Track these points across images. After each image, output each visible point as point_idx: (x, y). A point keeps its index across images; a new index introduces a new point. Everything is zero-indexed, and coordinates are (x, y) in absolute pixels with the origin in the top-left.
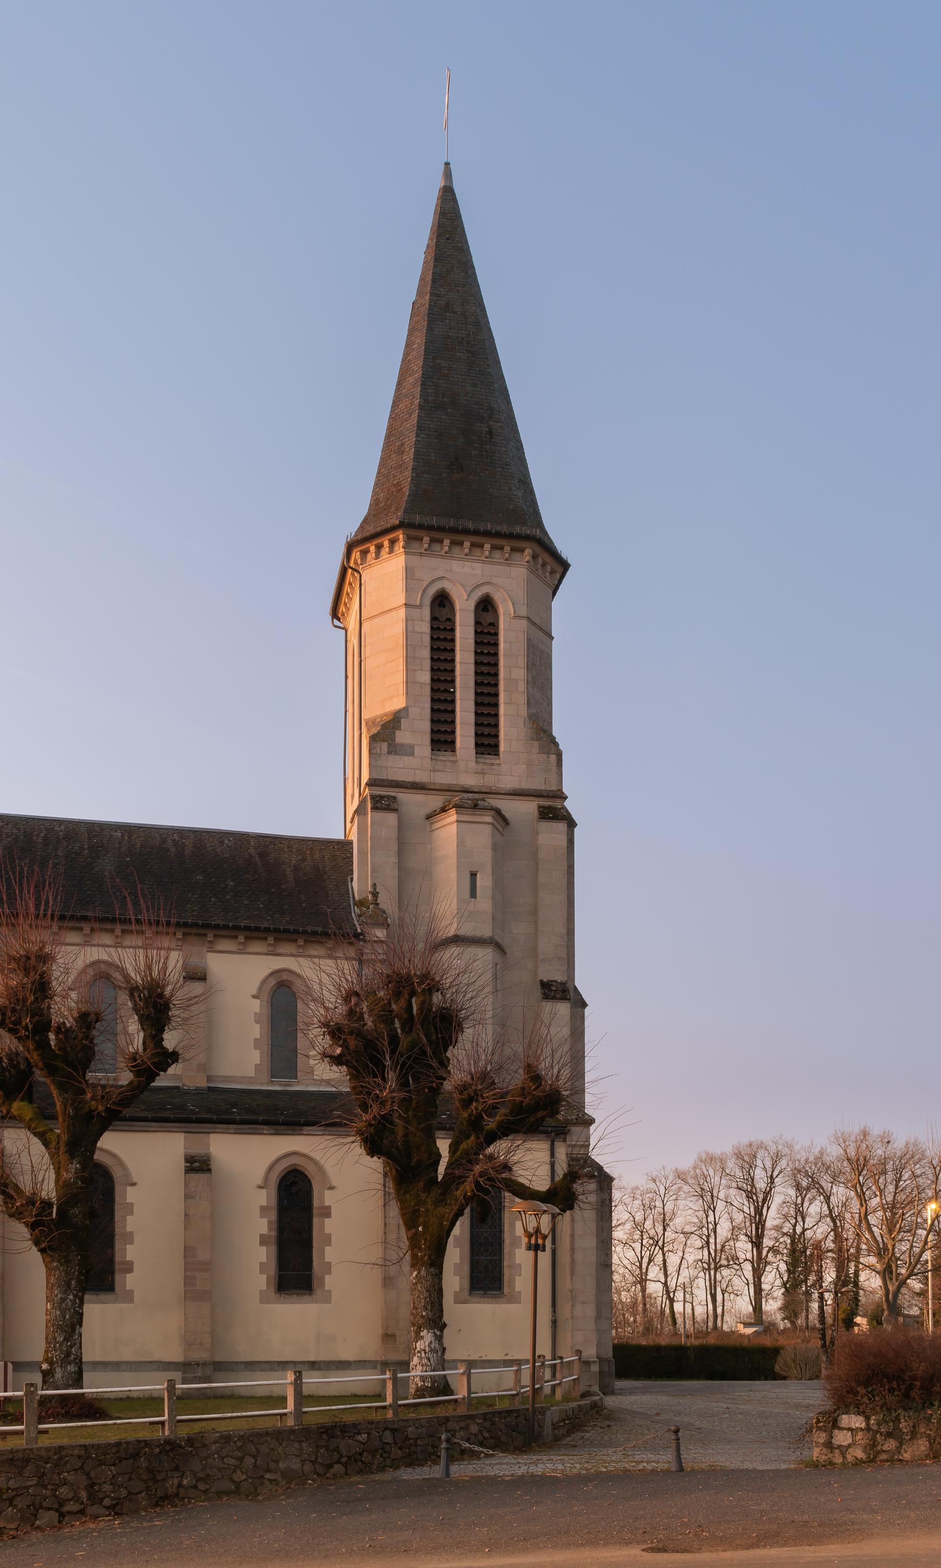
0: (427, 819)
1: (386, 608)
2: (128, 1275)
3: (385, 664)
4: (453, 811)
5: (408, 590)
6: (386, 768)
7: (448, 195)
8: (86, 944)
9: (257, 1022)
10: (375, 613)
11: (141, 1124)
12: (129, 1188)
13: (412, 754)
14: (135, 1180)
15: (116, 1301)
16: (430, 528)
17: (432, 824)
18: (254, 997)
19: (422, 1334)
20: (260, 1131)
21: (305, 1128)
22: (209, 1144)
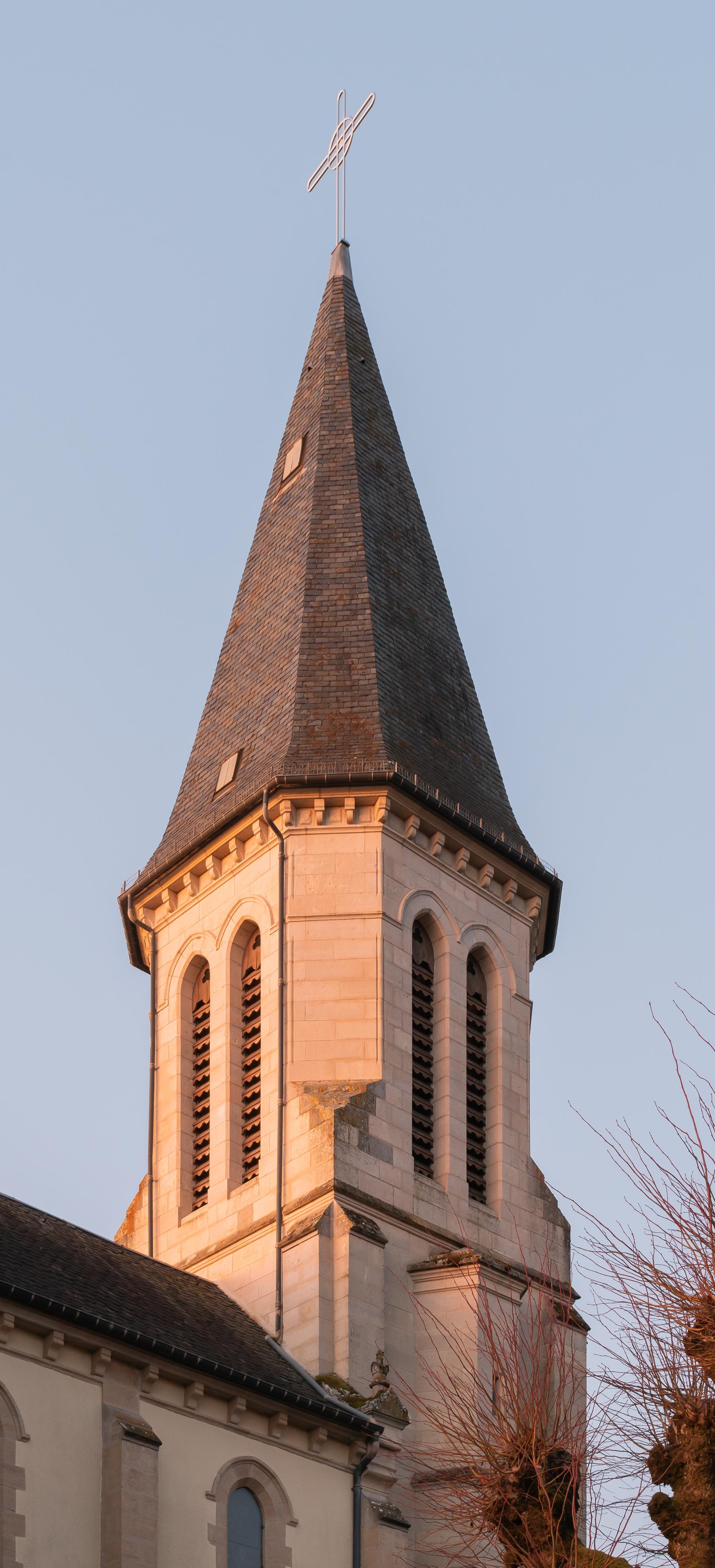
0: (410, 1272)
1: (340, 910)
3: (336, 1001)
4: (473, 1269)
5: (386, 893)
6: (357, 1170)
7: (343, 297)
9: (213, 1542)
10: (315, 911)
13: (390, 1161)
16: (430, 805)
17: (416, 1282)
18: (209, 1496)
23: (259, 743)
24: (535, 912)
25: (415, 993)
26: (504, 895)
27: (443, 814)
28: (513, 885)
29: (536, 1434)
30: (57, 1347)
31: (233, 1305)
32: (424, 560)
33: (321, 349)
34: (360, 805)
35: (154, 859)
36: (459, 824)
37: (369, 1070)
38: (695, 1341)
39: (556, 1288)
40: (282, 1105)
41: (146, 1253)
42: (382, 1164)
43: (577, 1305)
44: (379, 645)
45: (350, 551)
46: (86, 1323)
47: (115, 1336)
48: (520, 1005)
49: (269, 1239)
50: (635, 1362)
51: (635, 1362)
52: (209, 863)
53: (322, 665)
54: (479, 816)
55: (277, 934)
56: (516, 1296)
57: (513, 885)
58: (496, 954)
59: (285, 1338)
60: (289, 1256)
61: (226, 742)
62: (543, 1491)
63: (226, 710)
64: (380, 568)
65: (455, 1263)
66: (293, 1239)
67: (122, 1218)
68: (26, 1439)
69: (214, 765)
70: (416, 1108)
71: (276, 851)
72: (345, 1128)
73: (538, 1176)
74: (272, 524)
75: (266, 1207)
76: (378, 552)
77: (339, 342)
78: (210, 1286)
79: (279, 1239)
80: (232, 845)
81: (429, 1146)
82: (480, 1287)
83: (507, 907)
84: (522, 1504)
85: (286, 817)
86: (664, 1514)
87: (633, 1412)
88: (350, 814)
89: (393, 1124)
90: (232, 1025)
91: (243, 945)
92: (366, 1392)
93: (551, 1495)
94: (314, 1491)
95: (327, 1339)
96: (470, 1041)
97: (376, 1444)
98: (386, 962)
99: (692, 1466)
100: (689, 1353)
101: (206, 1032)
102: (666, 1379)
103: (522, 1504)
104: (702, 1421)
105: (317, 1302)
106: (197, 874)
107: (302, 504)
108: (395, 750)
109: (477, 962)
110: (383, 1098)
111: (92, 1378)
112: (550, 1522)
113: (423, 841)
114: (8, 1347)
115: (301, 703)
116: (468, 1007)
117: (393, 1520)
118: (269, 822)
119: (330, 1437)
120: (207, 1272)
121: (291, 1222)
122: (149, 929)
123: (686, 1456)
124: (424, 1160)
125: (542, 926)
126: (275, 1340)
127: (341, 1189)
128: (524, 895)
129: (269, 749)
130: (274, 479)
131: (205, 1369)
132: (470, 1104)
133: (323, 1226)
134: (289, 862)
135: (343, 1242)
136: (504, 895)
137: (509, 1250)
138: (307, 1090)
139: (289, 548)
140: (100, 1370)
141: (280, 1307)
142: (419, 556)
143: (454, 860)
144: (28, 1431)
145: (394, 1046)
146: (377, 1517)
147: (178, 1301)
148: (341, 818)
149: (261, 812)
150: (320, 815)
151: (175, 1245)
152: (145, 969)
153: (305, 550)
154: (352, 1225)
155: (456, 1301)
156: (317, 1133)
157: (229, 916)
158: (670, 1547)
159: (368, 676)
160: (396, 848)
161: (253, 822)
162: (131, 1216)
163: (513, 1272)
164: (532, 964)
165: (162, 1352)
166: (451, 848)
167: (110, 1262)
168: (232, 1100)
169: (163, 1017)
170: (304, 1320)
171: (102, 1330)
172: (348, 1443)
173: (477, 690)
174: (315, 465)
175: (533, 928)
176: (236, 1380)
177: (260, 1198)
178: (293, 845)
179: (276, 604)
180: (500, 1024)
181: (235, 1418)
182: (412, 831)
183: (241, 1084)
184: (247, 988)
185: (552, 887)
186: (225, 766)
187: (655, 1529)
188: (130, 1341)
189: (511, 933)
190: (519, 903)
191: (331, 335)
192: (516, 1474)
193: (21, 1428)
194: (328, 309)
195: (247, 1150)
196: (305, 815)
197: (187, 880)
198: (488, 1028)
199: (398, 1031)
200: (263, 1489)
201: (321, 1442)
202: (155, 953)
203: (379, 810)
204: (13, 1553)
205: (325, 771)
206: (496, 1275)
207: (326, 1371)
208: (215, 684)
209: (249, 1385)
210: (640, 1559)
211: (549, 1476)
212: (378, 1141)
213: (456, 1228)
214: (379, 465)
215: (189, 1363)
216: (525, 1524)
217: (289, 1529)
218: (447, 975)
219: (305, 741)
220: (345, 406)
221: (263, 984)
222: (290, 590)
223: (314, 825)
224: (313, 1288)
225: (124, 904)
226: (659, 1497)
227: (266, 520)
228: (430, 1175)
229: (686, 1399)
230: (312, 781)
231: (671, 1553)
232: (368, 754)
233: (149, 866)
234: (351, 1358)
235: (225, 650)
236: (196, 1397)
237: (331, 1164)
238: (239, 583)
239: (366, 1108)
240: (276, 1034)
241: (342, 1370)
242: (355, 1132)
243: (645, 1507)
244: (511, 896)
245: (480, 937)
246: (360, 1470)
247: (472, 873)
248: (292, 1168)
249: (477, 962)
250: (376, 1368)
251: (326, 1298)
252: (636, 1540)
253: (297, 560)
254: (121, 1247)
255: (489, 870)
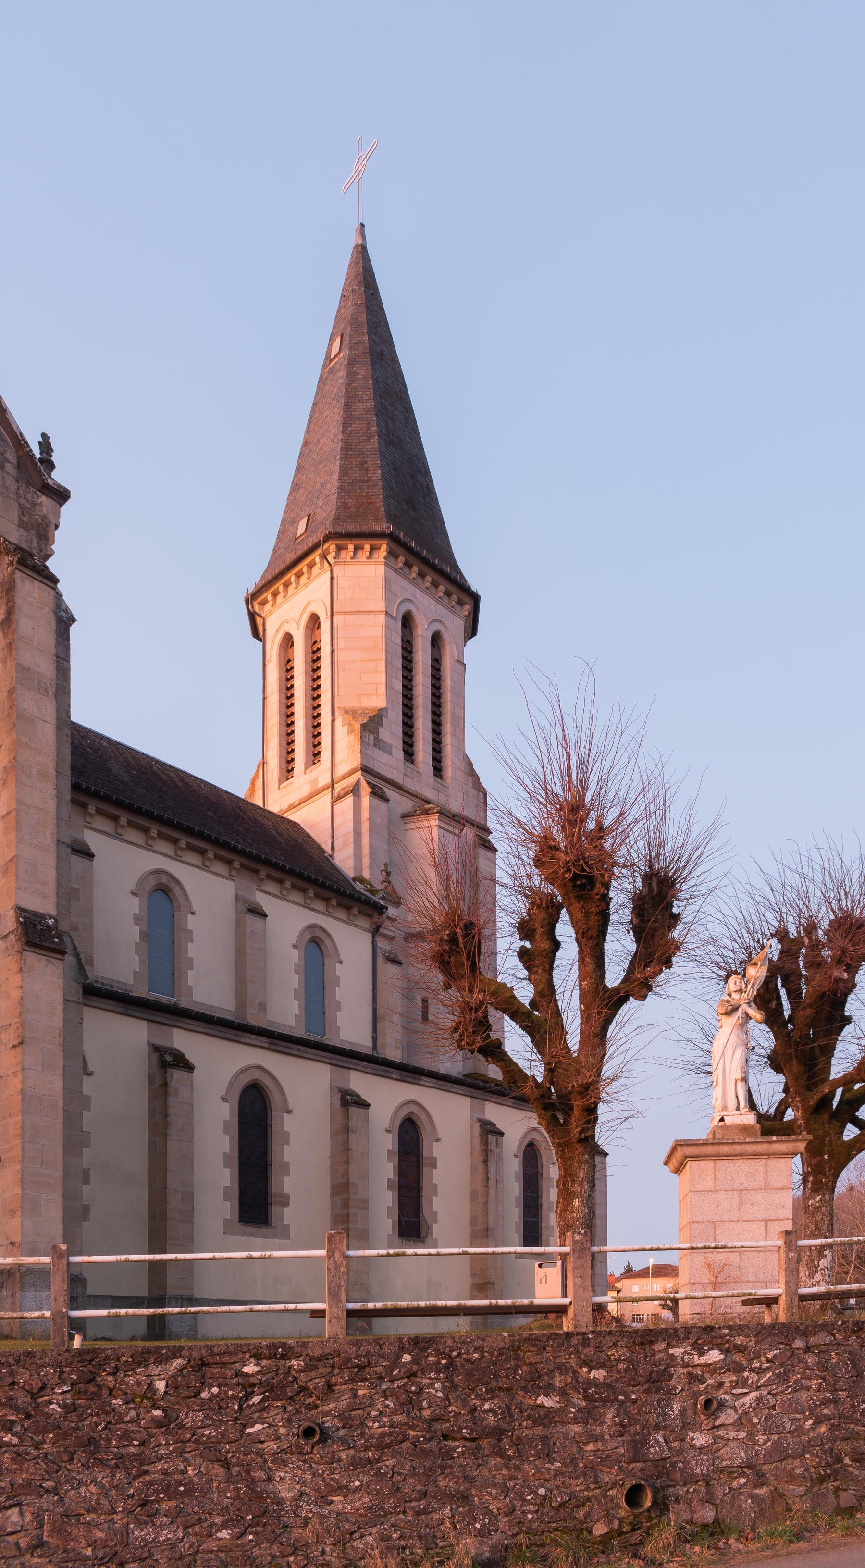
1: (362, 609)
2: (285, 1209)
3: (361, 661)
4: (437, 816)
5: (387, 599)
7: (362, 254)
8: (148, 847)
10: (350, 609)
11: (301, 1048)
12: (285, 1115)
13: (390, 754)
14: (291, 1107)
15: (275, 1236)
16: (410, 550)
17: (405, 823)
18: (294, 946)
19: (825, 1253)
20: (389, 1075)
21: (424, 1078)
22: (349, 1080)
23: (319, 511)
24: (466, 613)
25: (403, 657)
26: (450, 603)
27: (417, 555)
28: (455, 597)
29: (458, 911)
30: (210, 859)
31: (308, 836)
32: (406, 409)
33: (350, 285)
34: (373, 549)
35: (263, 576)
36: (425, 561)
37: (379, 702)
38: (538, 860)
39: (477, 827)
40: (333, 720)
41: (261, 805)
42: (386, 755)
43: (490, 837)
44: (382, 457)
45: (366, 403)
46: (225, 846)
47: (241, 853)
48: (459, 666)
49: (326, 797)
50: (510, 872)
51: (510, 872)
52: (293, 579)
53: (352, 467)
54: (436, 557)
55: (329, 622)
56: (457, 832)
57: (455, 597)
58: (446, 636)
59: (336, 855)
60: (338, 807)
61: (301, 509)
62: (461, 945)
63: (301, 491)
64: (382, 413)
65: (426, 813)
66: (339, 798)
67: (248, 784)
68: (193, 913)
69: (295, 522)
70: (404, 723)
71: (328, 574)
72: (367, 734)
73: (470, 764)
74: (325, 385)
75: (325, 780)
76: (381, 404)
77: (360, 282)
78: (296, 824)
79: (332, 798)
80: (305, 569)
81: (412, 745)
82: (439, 827)
83: (452, 609)
84: (451, 952)
85: (333, 554)
86: (526, 958)
87: (509, 899)
88: (368, 553)
89: (392, 732)
90: (306, 674)
91: (311, 627)
92: (379, 887)
93: (465, 947)
94: (351, 943)
95: (358, 856)
96: (433, 685)
97: (384, 916)
98: (388, 639)
99: (540, 931)
100: (537, 867)
101: (292, 677)
102: (526, 882)
103: (451, 952)
104: (544, 905)
105: (352, 834)
106: (287, 585)
107: (341, 374)
108: (391, 517)
109: (436, 640)
110: (387, 717)
111: (230, 877)
112: (465, 963)
113: (406, 570)
114: (183, 859)
115: (341, 488)
116: (432, 666)
117: (395, 961)
118: (324, 557)
119: (359, 912)
120: (294, 817)
121: (338, 787)
122: (261, 617)
123: (537, 925)
124: (409, 754)
125: (471, 621)
126: (330, 856)
127: (365, 770)
128: (461, 603)
129: (324, 515)
130: (326, 359)
131: (291, 873)
132: (433, 722)
133: (355, 790)
134: (335, 580)
135: (366, 800)
136: (450, 603)
137: (455, 806)
138: (346, 712)
139: (333, 399)
140: (234, 873)
141: (333, 837)
142: (404, 407)
143: (423, 582)
144: (194, 908)
145: (392, 688)
146: (385, 958)
147: (278, 833)
148: (363, 555)
149: (320, 551)
150: (351, 554)
151: (277, 800)
152: (260, 639)
153: (343, 400)
154: (370, 790)
155: (427, 833)
156: (352, 737)
157: (304, 610)
158: (529, 976)
159: (376, 474)
160: (392, 573)
161: (316, 557)
162: (253, 783)
163: (456, 818)
164: (465, 643)
165: (267, 863)
166: (421, 575)
167: (240, 810)
168: (306, 717)
169: (269, 668)
170: (345, 845)
171: (234, 850)
172: (370, 916)
173: (435, 485)
174: (347, 352)
175: (466, 622)
176: (308, 879)
177: (322, 774)
178: (337, 570)
179: (327, 431)
180: (449, 677)
181: (308, 901)
182: (401, 565)
183: (311, 707)
184: (314, 652)
185: (475, 599)
186: (301, 523)
187: (521, 966)
188: (250, 856)
189: (454, 625)
190: (458, 607)
191: (356, 277)
192: (448, 935)
193: (190, 906)
194: (354, 263)
195: (315, 746)
196: (343, 553)
197: (281, 589)
198: (442, 679)
199: (394, 679)
200: (324, 942)
201: (355, 915)
202: (264, 630)
203: (383, 552)
204: (187, 979)
205: (354, 528)
206: (447, 820)
207: (358, 875)
208: (295, 476)
209: (315, 882)
210: (513, 984)
211: (465, 936)
212: (384, 742)
213: (429, 794)
214: (382, 354)
215: (282, 869)
216: (452, 964)
217: (338, 965)
218: (420, 647)
219: (343, 511)
220: (363, 319)
221: (322, 650)
222: (334, 423)
223: (348, 559)
224: (350, 827)
225: (247, 601)
226: (523, 948)
227: (322, 381)
228: (413, 762)
229: (536, 894)
230: (347, 534)
231: (530, 979)
232: (377, 520)
233: (260, 580)
234: (371, 867)
235: (301, 456)
236: (287, 889)
237: (359, 755)
238: (307, 418)
239: (377, 723)
240: (330, 679)
241: (366, 874)
242: (372, 737)
243: (516, 954)
244: (454, 603)
245: (437, 626)
246: (375, 931)
247: (433, 589)
248: (338, 757)
249: (436, 640)
250: (384, 873)
251: (357, 833)
252: (512, 972)
253: (339, 405)
254: (247, 801)
255: (442, 588)
